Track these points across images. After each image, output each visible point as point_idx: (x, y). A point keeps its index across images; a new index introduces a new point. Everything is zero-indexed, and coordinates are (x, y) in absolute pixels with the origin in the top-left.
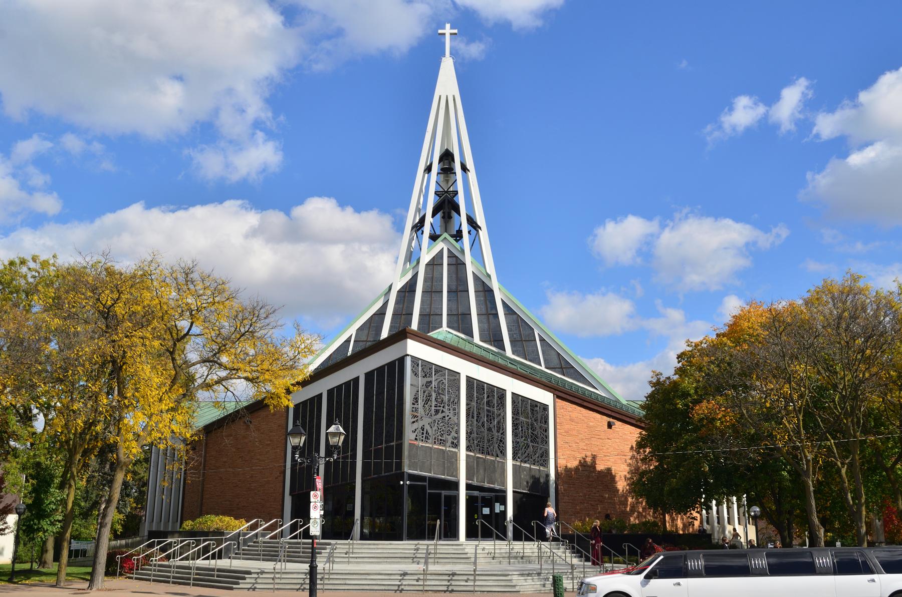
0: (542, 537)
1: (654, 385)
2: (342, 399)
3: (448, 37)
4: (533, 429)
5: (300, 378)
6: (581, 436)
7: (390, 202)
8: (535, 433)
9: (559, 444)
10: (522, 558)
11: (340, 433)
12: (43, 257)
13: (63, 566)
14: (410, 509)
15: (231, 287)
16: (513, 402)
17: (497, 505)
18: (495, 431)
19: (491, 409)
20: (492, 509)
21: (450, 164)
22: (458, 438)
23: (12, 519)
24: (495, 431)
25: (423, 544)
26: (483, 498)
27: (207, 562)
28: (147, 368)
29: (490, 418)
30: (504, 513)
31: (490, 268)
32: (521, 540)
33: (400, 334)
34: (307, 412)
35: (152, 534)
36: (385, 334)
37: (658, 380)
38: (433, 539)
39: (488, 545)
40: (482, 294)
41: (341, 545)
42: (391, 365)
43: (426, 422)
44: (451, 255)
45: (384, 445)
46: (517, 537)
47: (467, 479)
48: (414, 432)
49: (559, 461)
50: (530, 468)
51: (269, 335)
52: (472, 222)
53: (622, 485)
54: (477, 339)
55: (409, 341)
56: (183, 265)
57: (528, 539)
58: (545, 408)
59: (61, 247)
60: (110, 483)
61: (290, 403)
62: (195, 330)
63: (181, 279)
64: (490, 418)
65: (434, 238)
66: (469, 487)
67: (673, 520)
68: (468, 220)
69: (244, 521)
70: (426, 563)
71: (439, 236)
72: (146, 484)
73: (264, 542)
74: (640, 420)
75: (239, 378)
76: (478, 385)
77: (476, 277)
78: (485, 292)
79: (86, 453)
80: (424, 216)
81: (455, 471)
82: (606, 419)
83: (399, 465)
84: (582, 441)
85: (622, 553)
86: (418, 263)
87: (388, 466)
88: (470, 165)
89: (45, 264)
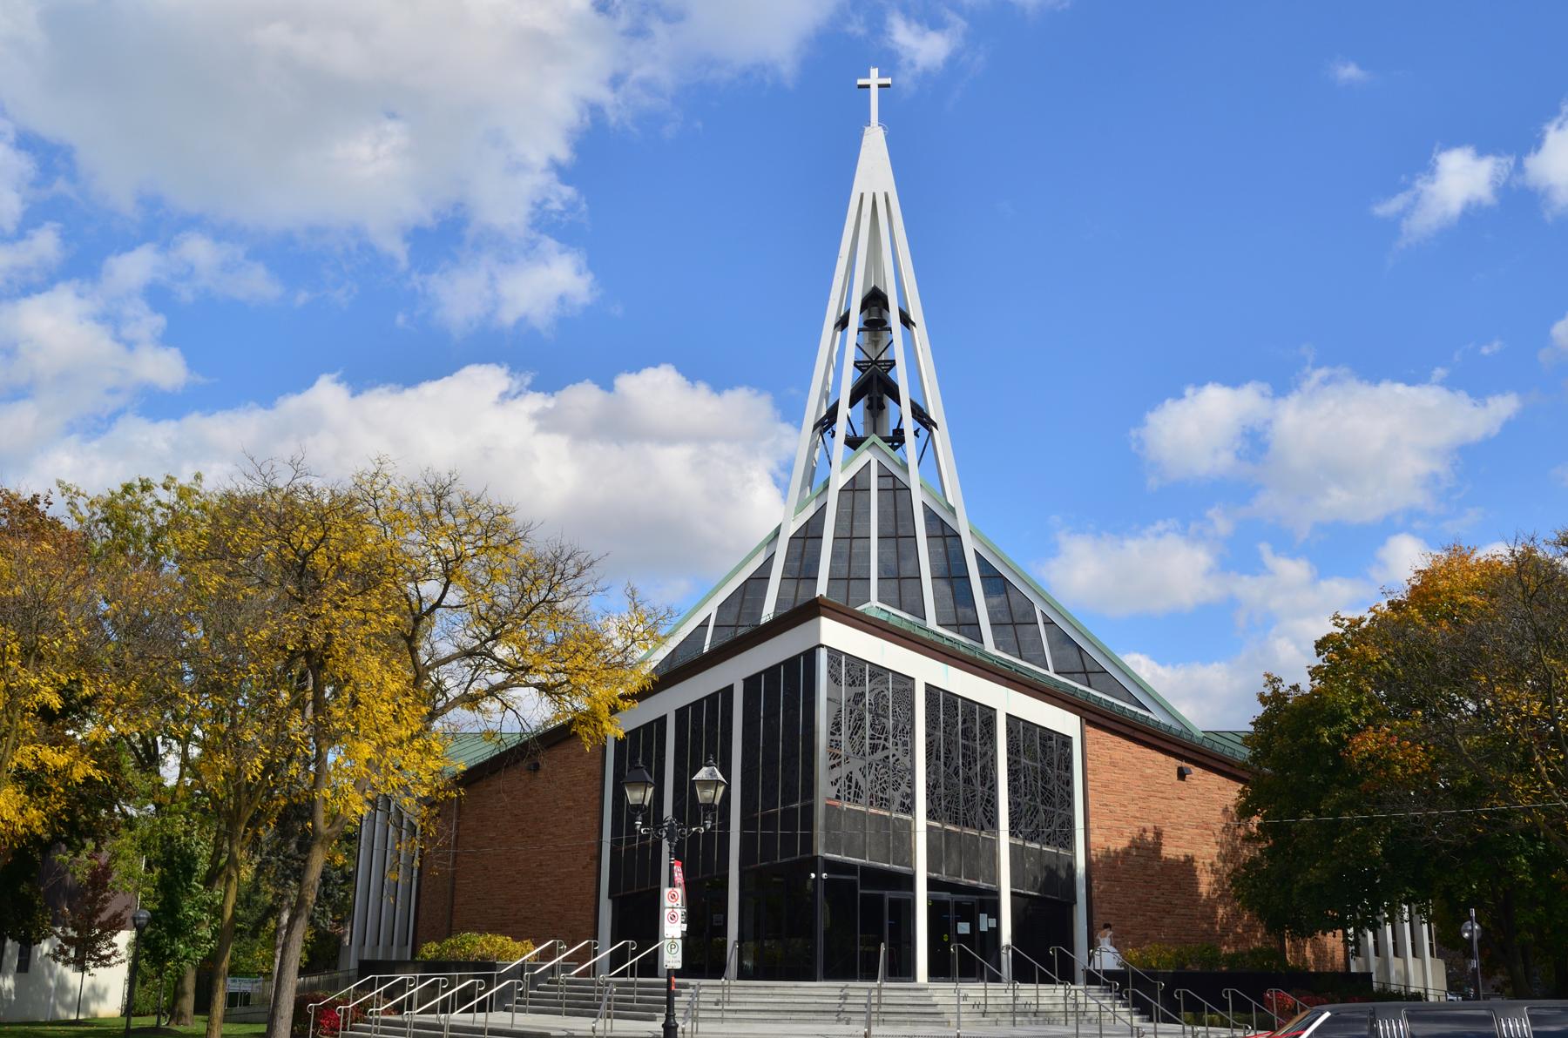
0: (1067, 976)
1: (1263, 699)
2: (703, 729)
3: (874, 91)
4: (1046, 780)
5: (634, 686)
6: (1131, 794)
7: (780, 383)
8: (1049, 787)
9: (1091, 808)
10: (1035, 1013)
11: (718, 782)
12: (185, 479)
13: (216, 1022)
14: (825, 922)
15: (518, 519)
16: (1009, 731)
17: (983, 917)
18: (977, 782)
19: (970, 743)
20: (974, 925)
21: (880, 313)
22: (911, 796)
23: (124, 938)
24: (977, 782)
25: (858, 990)
26: (958, 904)
27: (469, 1016)
28: (374, 663)
29: (969, 762)
30: (996, 932)
31: (954, 496)
32: (1033, 982)
33: (805, 611)
34: (640, 748)
35: (365, 967)
36: (768, 612)
37: (1276, 691)
38: (874, 978)
39: (974, 990)
40: (940, 541)
41: (707, 989)
42: (791, 663)
43: (855, 765)
44: (884, 474)
46: (1023, 974)
47: (929, 869)
48: (834, 784)
49: (1092, 839)
50: (1041, 851)
51: (580, 607)
52: (920, 414)
53: (1205, 884)
55: (824, 621)
56: (432, 481)
57: (1046, 980)
58: (1066, 741)
59: (220, 456)
60: (299, 874)
61: (615, 730)
62: (452, 598)
63: (429, 507)
64: (969, 762)
66: (932, 884)
67: (1298, 949)
69: (530, 945)
70: (869, 1024)
71: (862, 440)
72: (349, 878)
73: (569, 982)
74: (1243, 766)
75: (527, 685)
76: (945, 700)
77: (931, 516)
78: (944, 534)
79: (254, 822)
80: (837, 404)
81: (908, 856)
82: (1174, 763)
83: (808, 841)
84: (1118, 803)
85: (1223, 1006)
86: (826, 487)
87: (789, 841)
88: (916, 314)
89: (184, 493)
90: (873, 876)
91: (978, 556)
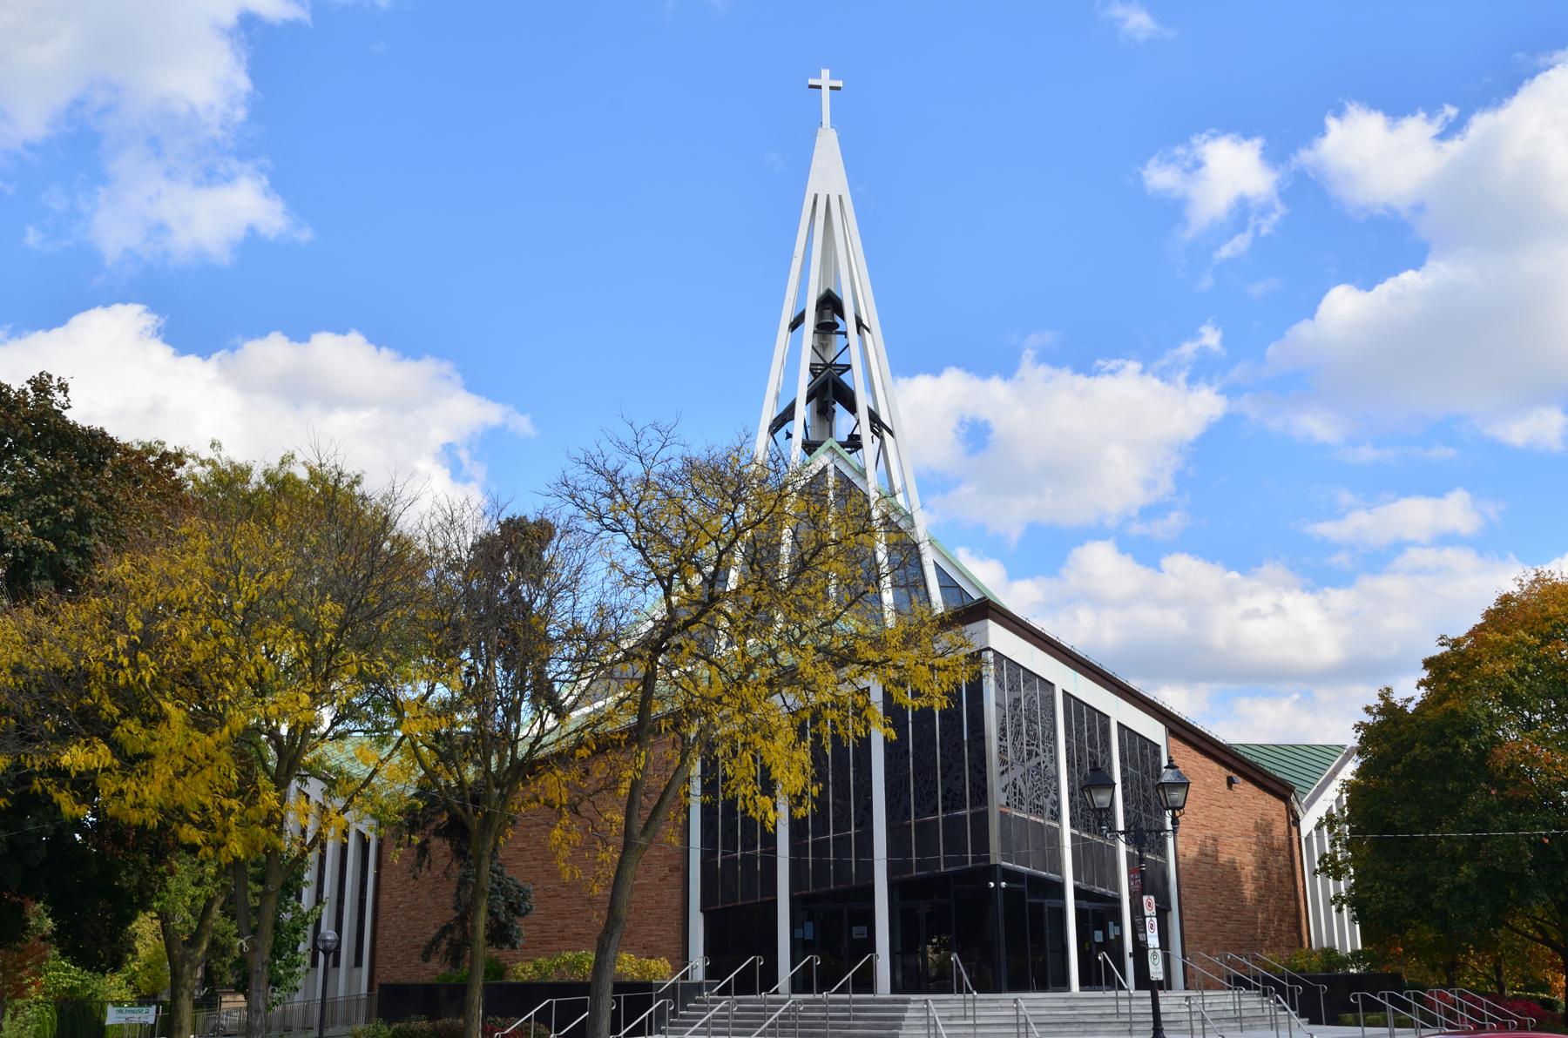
3: (826, 92)
14: (990, 928)
20: (1106, 935)
22: (1057, 803)
30: (1120, 938)
45: (940, 815)
48: (1004, 790)
53: (1249, 890)
55: (990, 622)
58: (1156, 748)
71: (819, 444)
82: (1225, 772)
85: (1354, 1009)
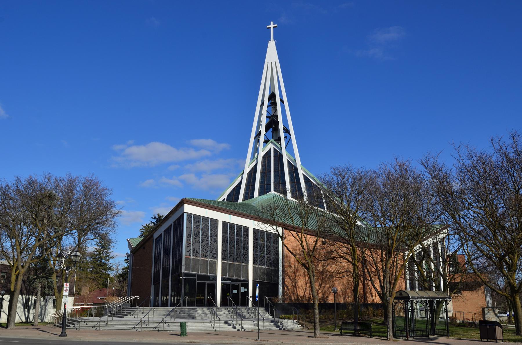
14: (197, 293)
30: (247, 293)
54: (289, 195)
55: (185, 205)
65: (266, 142)
66: (223, 279)
68: (284, 129)
77: (289, 163)
78: (293, 169)
90: (207, 278)
91: (305, 177)
